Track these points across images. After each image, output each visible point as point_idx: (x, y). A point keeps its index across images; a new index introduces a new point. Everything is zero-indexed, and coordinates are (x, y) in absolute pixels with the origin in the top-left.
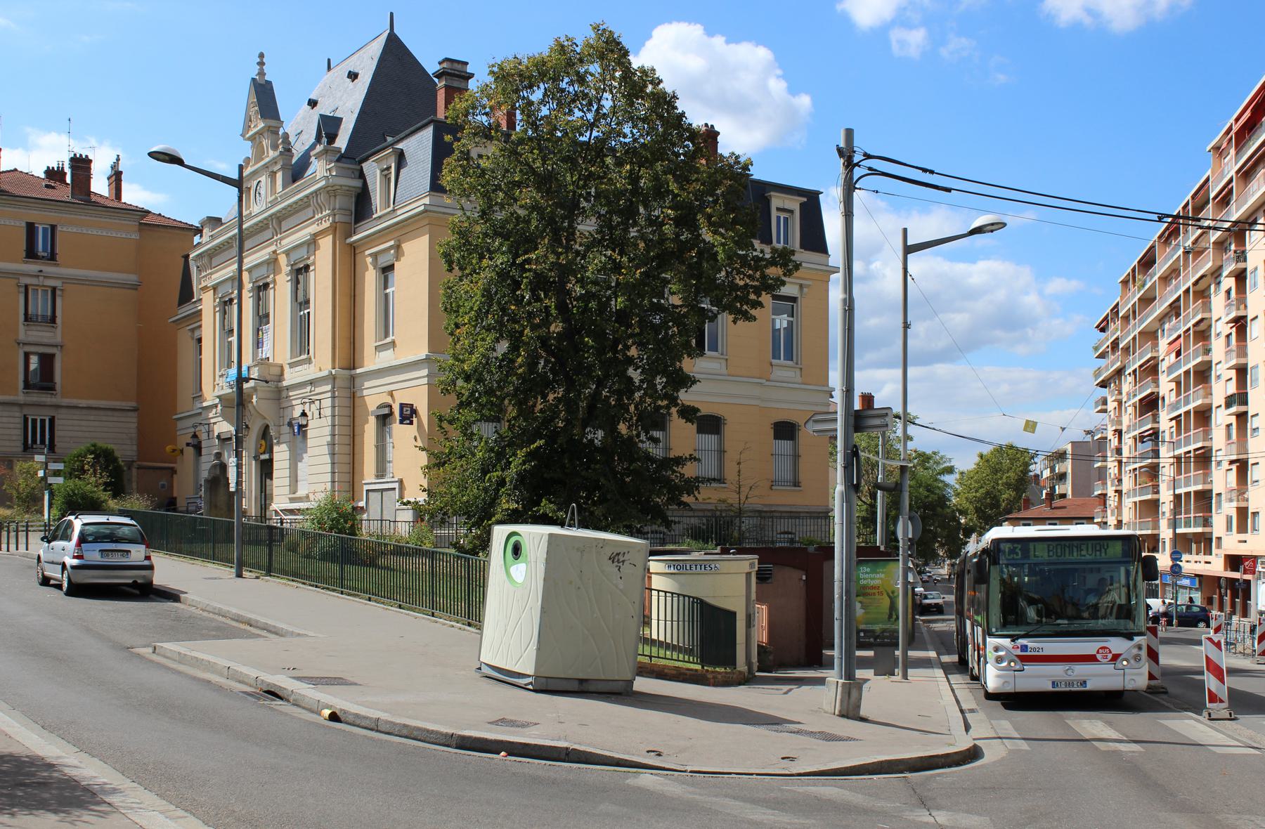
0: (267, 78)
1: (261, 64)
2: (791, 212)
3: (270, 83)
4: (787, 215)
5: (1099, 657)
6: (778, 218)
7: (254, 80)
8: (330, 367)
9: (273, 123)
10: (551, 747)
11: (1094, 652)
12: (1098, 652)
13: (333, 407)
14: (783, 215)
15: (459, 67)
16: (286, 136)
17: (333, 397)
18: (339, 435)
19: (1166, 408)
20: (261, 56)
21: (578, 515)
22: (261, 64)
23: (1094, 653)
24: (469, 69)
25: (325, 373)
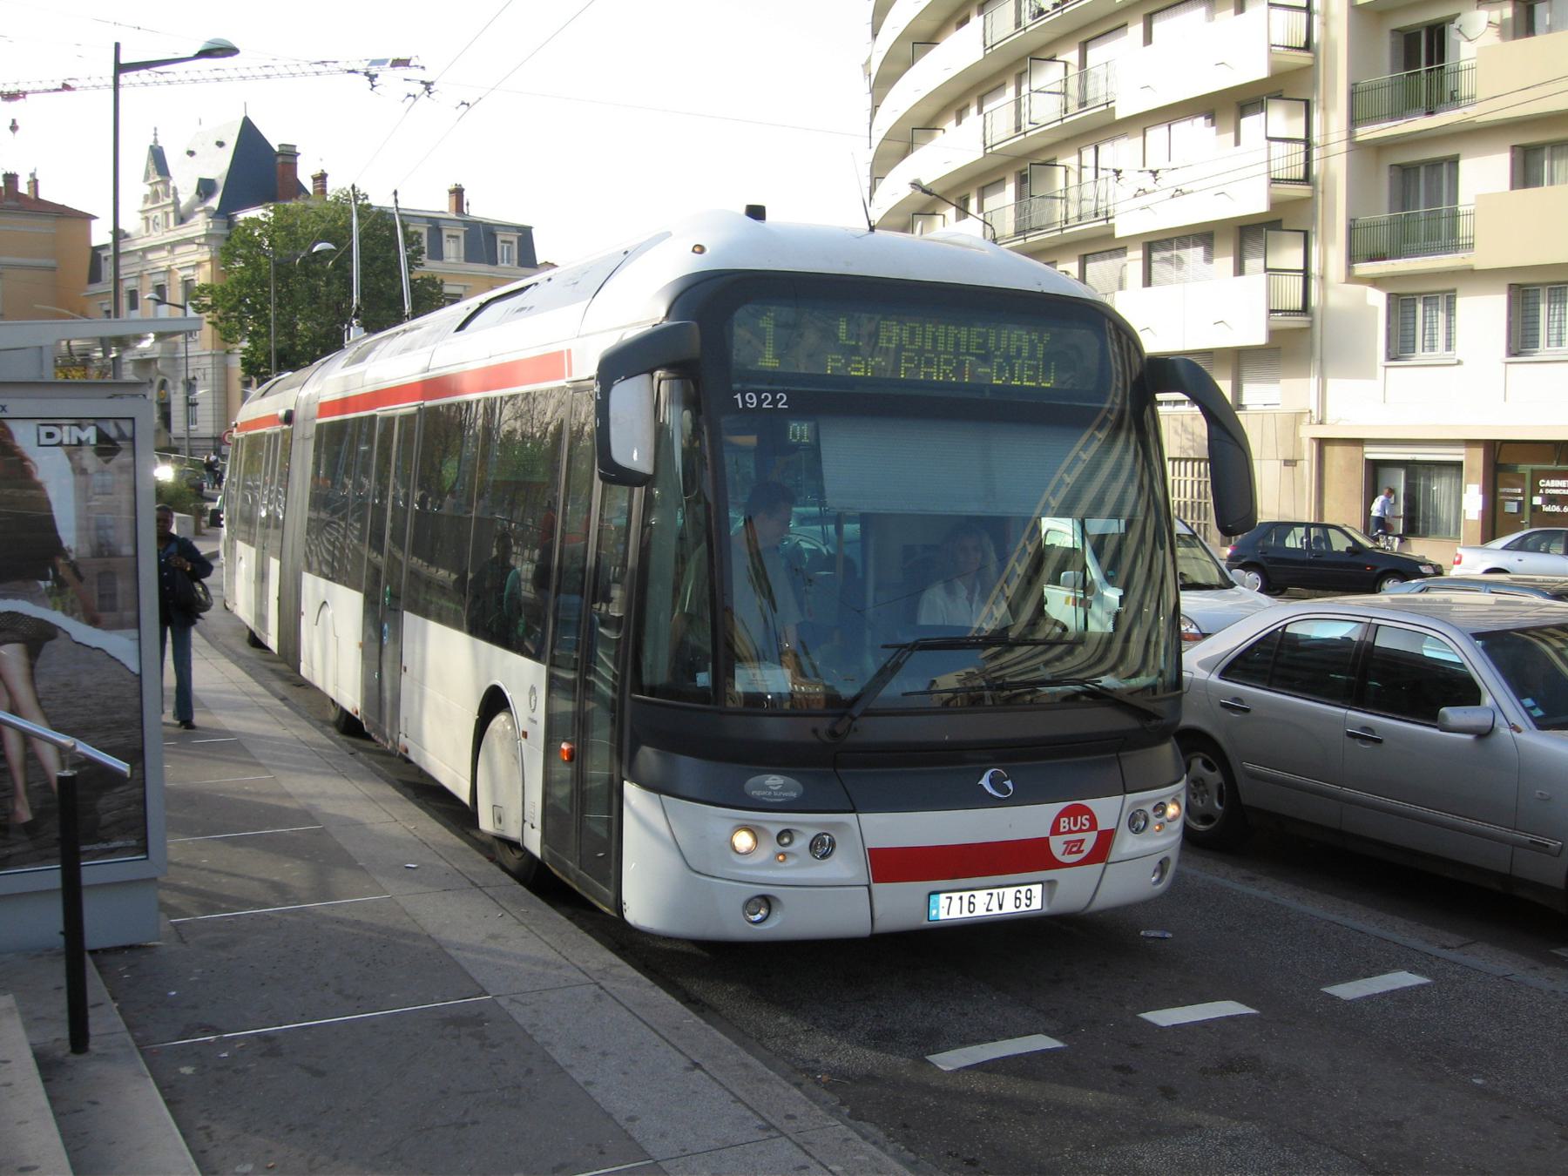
0: (160, 144)
1: (155, 135)
2: (511, 243)
3: (161, 148)
4: (508, 245)
5: (1057, 846)
6: (503, 248)
7: (151, 147)
8: (210, 348)
9: (166, 178)
10: (95, 759)
11: (1043, 831)
12: (1055, 830)
13: (213, 374)
14: (506, 246)
15: (289, 149)
16: (175, 189)
17: (213, 368)
18: (1346, 714)
19: (467, 597)
20: (155, 129)
21: (555, 499)
22: (155, 135)
23: (1046, 834)
24: (298, 151)
25: (209, 353)
